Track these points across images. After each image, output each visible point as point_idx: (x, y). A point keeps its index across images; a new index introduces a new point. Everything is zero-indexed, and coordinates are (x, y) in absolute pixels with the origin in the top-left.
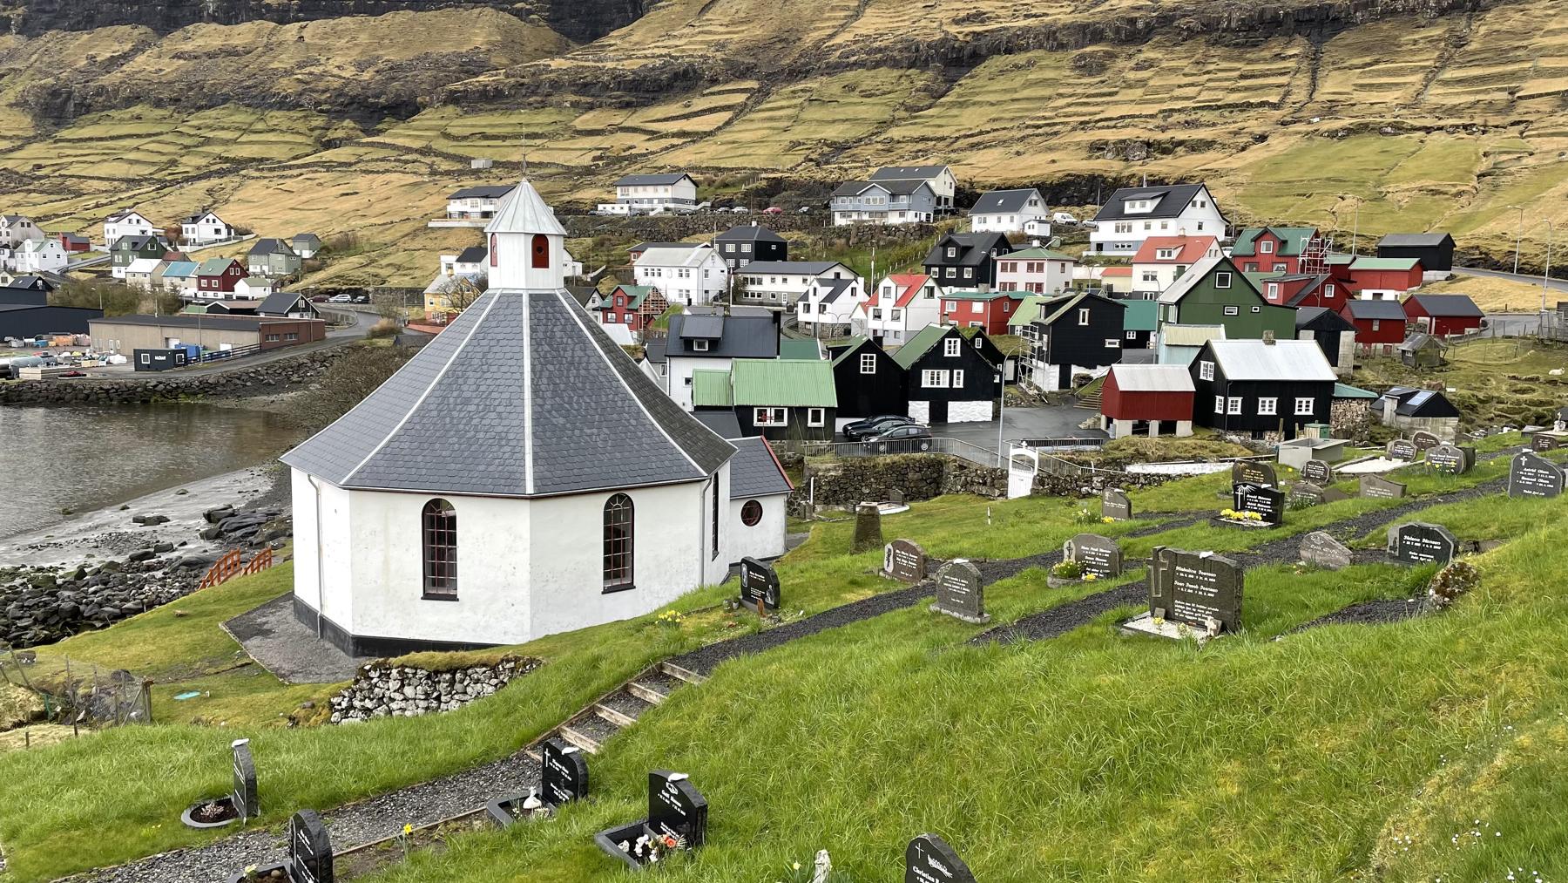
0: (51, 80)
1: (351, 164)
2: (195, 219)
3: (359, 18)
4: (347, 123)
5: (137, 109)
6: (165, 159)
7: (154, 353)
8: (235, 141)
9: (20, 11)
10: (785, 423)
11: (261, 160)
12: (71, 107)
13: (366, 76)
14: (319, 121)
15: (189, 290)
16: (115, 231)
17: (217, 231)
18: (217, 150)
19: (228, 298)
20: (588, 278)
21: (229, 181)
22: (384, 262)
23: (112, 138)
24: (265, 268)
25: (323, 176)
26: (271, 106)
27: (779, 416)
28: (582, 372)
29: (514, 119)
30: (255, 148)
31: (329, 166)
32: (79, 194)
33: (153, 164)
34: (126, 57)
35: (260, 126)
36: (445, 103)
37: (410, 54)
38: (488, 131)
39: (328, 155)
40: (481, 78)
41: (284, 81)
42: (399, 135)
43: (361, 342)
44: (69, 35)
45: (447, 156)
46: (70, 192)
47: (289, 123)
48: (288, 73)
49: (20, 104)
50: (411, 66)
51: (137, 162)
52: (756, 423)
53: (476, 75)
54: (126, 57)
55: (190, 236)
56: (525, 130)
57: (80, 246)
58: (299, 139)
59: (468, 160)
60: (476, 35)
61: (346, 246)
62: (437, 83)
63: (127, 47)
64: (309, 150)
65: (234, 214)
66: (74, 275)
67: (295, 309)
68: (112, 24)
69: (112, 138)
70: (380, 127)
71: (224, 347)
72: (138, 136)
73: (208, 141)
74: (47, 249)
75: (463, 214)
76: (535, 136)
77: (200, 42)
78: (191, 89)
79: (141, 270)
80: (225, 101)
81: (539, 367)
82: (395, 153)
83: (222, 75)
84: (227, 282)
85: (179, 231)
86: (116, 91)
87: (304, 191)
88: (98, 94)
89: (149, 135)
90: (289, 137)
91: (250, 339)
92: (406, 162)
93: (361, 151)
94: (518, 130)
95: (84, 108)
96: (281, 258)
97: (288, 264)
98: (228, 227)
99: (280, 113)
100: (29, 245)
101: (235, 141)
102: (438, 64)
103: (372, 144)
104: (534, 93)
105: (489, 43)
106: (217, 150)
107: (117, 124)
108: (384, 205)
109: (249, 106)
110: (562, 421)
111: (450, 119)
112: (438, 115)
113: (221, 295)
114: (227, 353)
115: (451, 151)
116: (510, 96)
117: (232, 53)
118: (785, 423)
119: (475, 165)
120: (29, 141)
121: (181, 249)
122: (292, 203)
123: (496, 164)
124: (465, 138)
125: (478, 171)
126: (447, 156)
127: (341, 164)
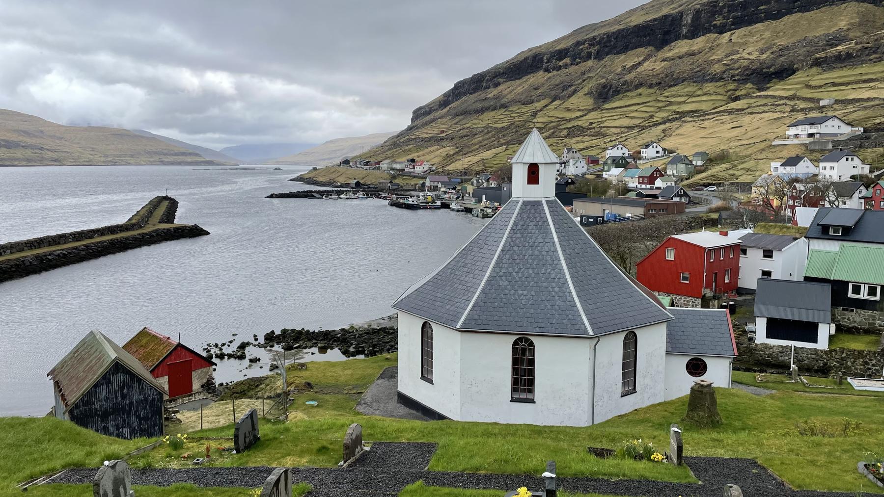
0: (604, 80)
1: (743, 110)
2: (647, 146)
3: (767, 23)
4: (749, 85)
5: (640, 91)
6: (648, 115)
7: (589, 217)
8: (684, 102)
9: (596, 48)
10: (878, 298)
11: (696, 111)
12: (611, 93)
13: (764, 56)
14: (732, 86)
15: (633, 184)
16: (610, 153)
17: (658, 152)
18: (674, 108)
19: (651, 188)
20: (873, 176)
21: (674, 125)
22: (740, 167)
23: (626, 106)
24: (675, 172)
25: (727, 117)
26: (707, 81)
27: (872, 291)
28: (537, 253)
29: (858, 71)
30: (694, 105)
31: (730, 112)
32: (605, 136)
33: (642, 118)
34: (640, 64)
35: (699, 92)
36: (811, 66)
37: (794, 40)
38: (837, 81)
39: (733, 105)
40: (839, 48)
41: (716, 66)
42: (779, 89)
43: (701, 215)
44: (616, 57)
45: (805, 99)
46: (602, 135)
47: (715, 89)
48: (719, 61)
49: (589, 94)
50: (794, 46)
51: (635, 117)
52: (850, 295)
53: (837, 46)
54: (640, 64)
55: (644, 155)
56: (864, 77)
57: (594, 161)
58: (719, 97)
59: (818, 100)
60: (842, 20)
61: (722, 157)
62: (810, 53)
63: (641, 59)
64: (723, 103)
65: (668, 144)
66: (587, 176)
67: (678, 195)
68: (636, 48)
69: (626, 106)
70: (768, 85)
71: (628, 215)
72: (638, 104)
73: (671, 103)
74: (578, 164)
75: (796, 136)
76: (871, 80)
77: (676, 51)
78: (667, 76)
79: (614, 174)
80: (683, 81)
81: (507, 248)
82: (772, 100)
83: (686, 66)
84: (652, 179)
85: (639, 152)
86: (632, 82)
87: (713, 127)
88: (624, 85)
89: (643, 103)
90: (714, 97)
91: (640, 211)
92: (778, 105)
93: (752, 101)
94: (859, 78)
95: (617, 92)
96: (683, 166)
97: (686, 169)
98: (664, 150)
99: (710, 84)
100: (571, 162)
101: (684, 102)
102: (812, 43)
103: (760, 97)
104: (875, 52)
105: (850, 24)
106: (674, 108)
107: (631, 98)
108: (754, 132)
109: (695, 82)
110: (506, 283)
111: (813, 76)
112: (806, 74)
113: (648, 186)
114: (628, 218)
115: (809, 96)
116: (857, 56)
117: (693, 54)
118: (878, 298)
119: (822, 103)
120: (590, 111)
121: (638, 162)
122: (702, 135)
123: (837, 102)
124: (820, 87)
125: (824, 107)
126: (805, 99)
127: (737, 110)
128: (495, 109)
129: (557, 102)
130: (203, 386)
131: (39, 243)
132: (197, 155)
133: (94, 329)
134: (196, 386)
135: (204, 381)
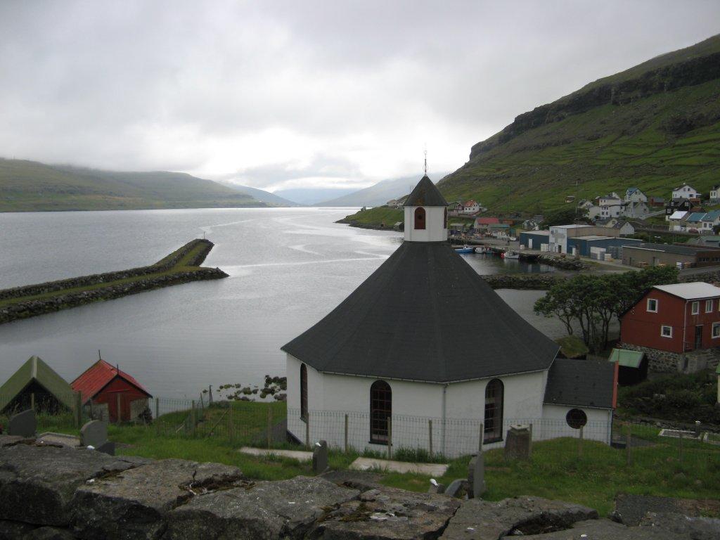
128: (556, 145)
129: (625, 138)
130: (140, 416)
131: (73, 283)
132: (249, 197)
133: (532, 309)
134: (134, 415)
135: (141, 411)
